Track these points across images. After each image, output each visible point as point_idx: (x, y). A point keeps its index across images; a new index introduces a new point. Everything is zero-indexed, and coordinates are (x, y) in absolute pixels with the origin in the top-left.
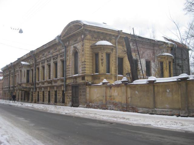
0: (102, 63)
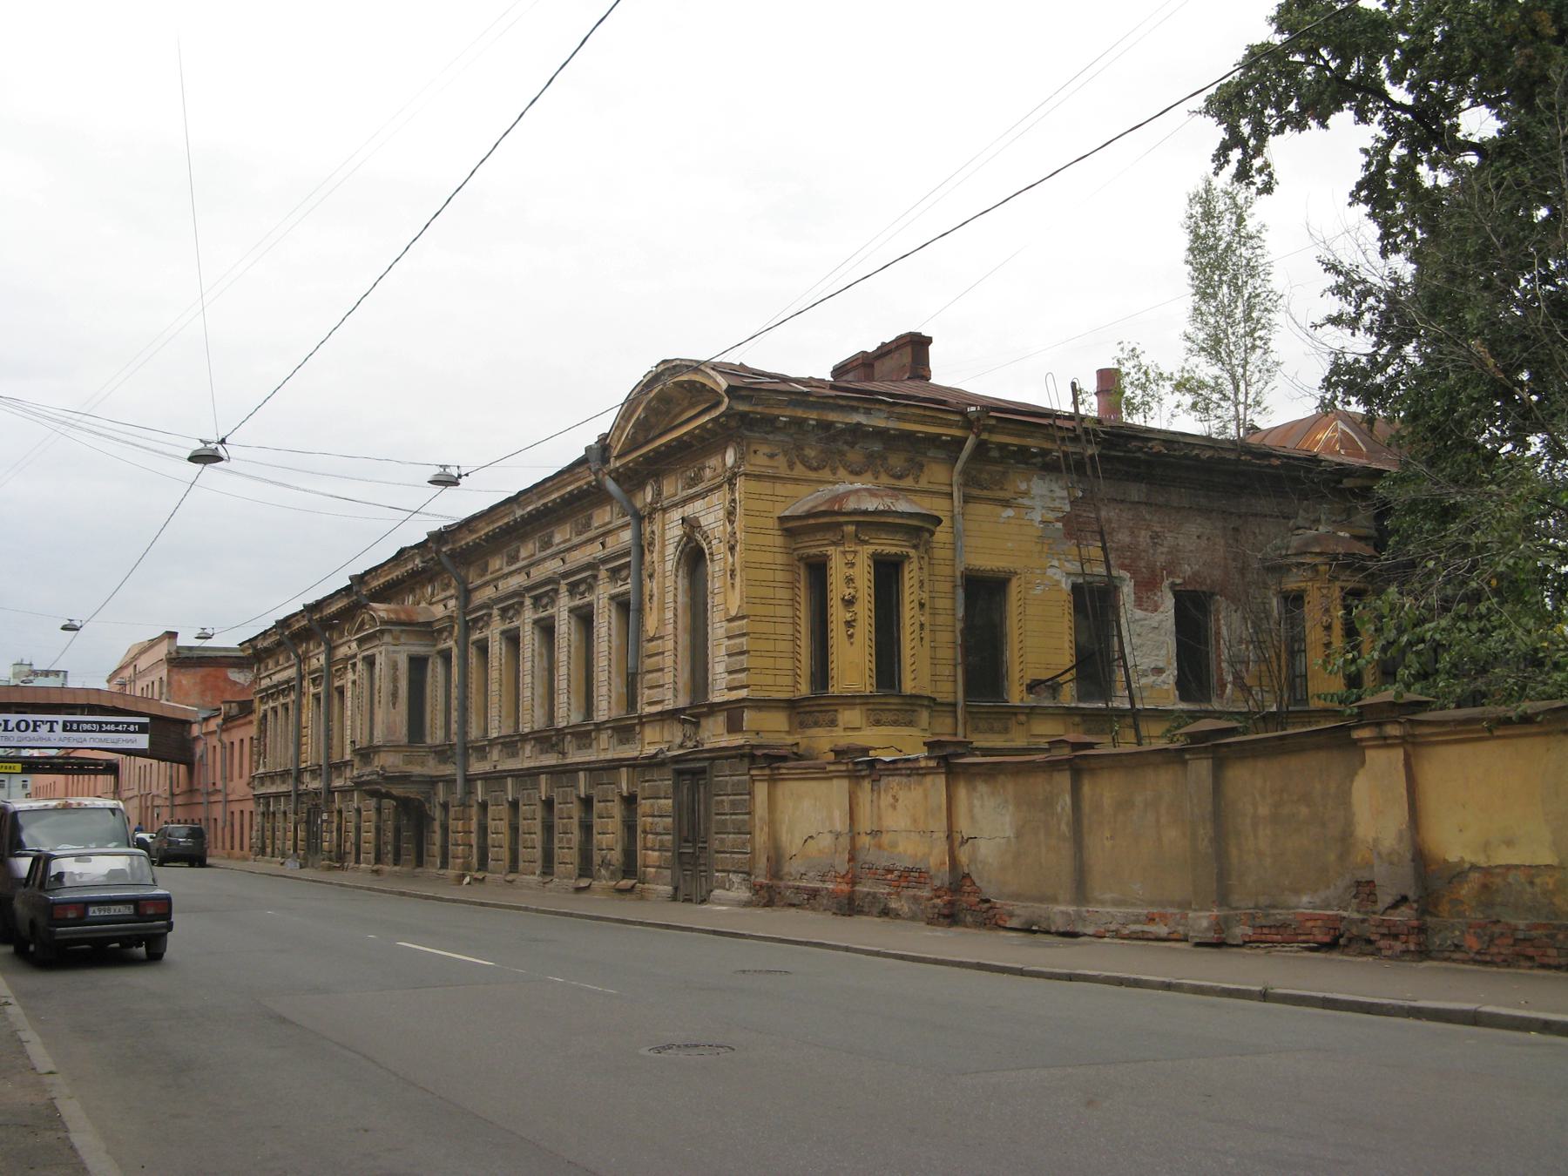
0: (849, 624)
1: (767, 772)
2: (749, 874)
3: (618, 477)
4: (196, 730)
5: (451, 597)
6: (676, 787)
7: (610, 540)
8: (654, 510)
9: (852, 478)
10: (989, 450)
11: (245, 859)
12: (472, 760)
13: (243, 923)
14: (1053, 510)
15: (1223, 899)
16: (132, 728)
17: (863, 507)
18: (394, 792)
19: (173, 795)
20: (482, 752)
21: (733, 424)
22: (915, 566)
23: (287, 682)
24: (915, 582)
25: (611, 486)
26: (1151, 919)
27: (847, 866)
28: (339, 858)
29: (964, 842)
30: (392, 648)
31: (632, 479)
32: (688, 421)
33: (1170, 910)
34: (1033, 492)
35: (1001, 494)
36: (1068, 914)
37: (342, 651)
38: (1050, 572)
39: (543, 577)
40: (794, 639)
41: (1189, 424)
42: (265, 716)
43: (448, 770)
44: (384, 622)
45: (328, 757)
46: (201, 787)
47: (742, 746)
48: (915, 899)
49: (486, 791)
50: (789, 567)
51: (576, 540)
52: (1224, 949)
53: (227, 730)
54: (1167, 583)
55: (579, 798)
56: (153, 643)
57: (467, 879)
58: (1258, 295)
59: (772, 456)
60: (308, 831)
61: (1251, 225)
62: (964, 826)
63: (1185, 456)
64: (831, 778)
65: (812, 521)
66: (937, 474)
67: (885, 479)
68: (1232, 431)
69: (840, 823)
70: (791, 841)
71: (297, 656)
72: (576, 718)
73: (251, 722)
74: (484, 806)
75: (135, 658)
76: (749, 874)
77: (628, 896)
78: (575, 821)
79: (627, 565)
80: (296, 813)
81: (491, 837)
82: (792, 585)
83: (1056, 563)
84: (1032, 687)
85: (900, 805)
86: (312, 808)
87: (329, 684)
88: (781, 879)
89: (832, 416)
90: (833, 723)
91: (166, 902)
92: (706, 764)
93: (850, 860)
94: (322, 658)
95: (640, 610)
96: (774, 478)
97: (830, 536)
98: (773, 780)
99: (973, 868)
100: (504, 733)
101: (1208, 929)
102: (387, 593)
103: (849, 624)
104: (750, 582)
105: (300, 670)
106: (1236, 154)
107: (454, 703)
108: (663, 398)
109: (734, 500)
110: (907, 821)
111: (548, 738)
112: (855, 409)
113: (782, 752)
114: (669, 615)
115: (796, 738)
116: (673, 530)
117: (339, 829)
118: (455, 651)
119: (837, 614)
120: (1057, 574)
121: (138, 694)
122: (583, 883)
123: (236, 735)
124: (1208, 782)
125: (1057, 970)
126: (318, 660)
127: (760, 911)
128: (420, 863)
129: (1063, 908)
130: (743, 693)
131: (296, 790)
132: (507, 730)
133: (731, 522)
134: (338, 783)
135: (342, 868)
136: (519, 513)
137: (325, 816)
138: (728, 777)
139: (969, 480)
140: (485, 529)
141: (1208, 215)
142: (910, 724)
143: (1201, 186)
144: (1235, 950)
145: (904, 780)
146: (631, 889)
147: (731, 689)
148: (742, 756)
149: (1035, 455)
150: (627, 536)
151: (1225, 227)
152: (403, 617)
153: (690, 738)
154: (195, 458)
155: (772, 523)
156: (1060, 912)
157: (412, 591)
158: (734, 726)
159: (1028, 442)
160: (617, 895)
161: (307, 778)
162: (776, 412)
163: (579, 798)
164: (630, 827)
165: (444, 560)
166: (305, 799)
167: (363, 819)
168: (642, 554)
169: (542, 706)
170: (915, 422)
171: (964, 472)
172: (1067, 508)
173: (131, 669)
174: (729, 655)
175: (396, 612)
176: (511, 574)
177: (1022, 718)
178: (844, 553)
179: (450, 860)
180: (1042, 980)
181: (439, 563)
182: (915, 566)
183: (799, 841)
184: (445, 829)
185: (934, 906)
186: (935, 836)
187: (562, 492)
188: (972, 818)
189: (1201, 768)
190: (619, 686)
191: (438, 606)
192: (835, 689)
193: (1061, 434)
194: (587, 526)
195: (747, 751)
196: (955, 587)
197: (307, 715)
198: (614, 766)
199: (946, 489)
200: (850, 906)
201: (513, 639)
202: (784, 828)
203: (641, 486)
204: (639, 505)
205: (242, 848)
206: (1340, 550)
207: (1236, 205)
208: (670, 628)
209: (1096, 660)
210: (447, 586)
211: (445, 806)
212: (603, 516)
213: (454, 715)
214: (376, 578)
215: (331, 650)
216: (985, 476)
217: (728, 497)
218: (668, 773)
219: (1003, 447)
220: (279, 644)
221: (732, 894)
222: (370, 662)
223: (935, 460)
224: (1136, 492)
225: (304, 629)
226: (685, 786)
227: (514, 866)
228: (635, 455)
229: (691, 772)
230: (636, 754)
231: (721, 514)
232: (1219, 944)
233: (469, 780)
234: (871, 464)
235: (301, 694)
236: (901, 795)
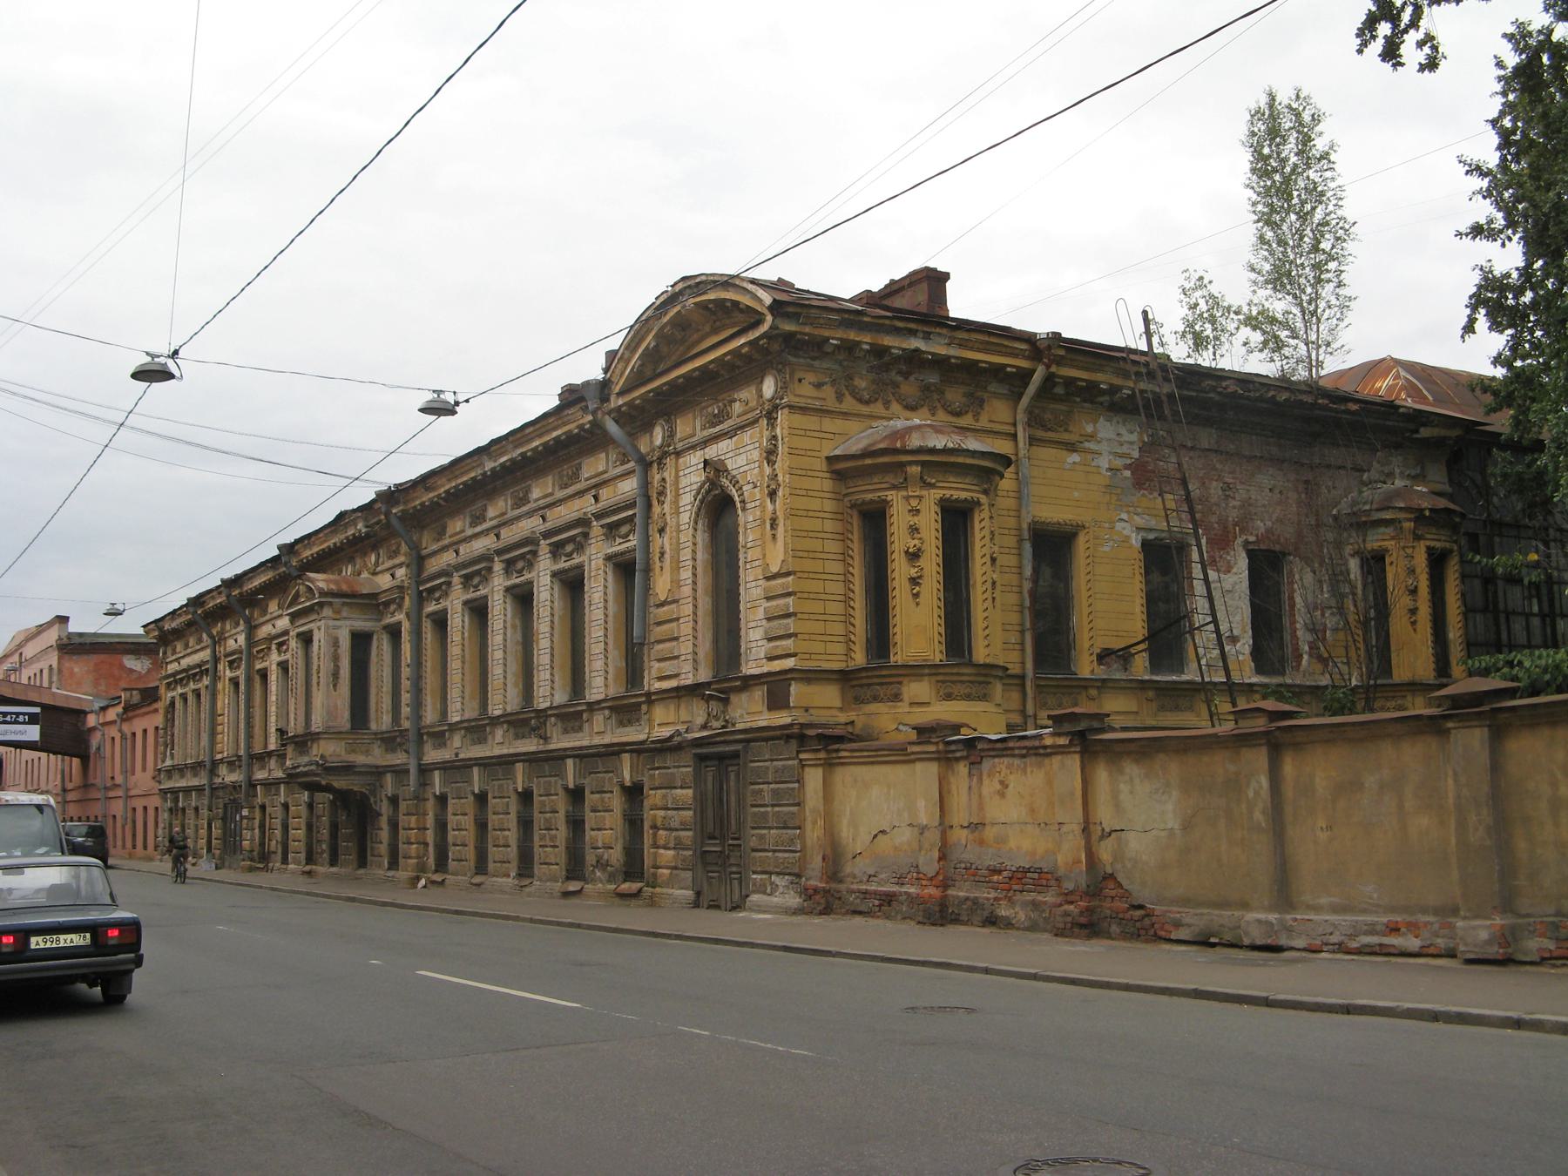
0: (914, 581)
1: (822, 755)
2: (799, 876)
3: (621, 417)
4: (92, 721)
5: (400, 565)
6: (698, 775)
7: (605, 493)
8: (665, 454)
9: (908, 414)
10: (1055, 384)
11: (150, 859)
12: (428, 747)
13: (232, 954)
14: (1121, 456)
15: (1507, 904)
16: (21, 718)
17: (930, 445)
18: (336, 784)
19: (64, 790)
20: (440, 738)
21: (776, 347)
22: (986, 514)
23: (199, 666)
24: (986, 532)
25: (612, 427)
26: (1394, 929)
27: (936, 866)
28: (262, 858)
29: (1106, 835)
30: (331, 623)
31: (638, 419)
32: (717, 344)
33: (1423, 918)
34: (1100, 435)
35: (1066, 437)
36: (1269, 923)
37: (265, 631)
38: (1119, 526)
39: (517, 538)
40: (847, 600)
41: (1261, 365)
42: (173, 704)
43: (398, 758)
44: (323, 593)
45: (249, 746)
46: (98, 781)
47: (790, 725)
48: (1035, 905)
49: (444, 782)
50: (839, 516)
51: (560, 494)
52: (1513, 968)
53: (128, 719)
54: (1239, 541)
55: (566, 789)
56: (41, 629)
57: (423, 882)
58: (1327, 224)
59: (818, 386)
60: (225, 828)
61: (1320, 145)
62: (1105, 815)
63: (1261, 399)
64: (913, 761)
65: (868, 461)
66: (998, 411)
67: (942, 415)
68: (1302, 374)
69: (925, 812)
70: (855, 836)
71: (211, 637)
72: (560, 698)
73: (156, 711)
74: (442, 800)
75: (20, 646)
76: (799, 876)
77: (634, 902)
78: (561, 815)
79: (630, 519)
80: (210, 810)
81: (451, 835)
82: (844, 537)
83: (1124, 516)
84: (1104, 656)
85: (1010, 791)
86: (230, 803)
87: (250, 666)
88: (841, 881)
89: (888, 341)
90: (897, 697)
91: (132, 929)
92: (739, 747)
93: (940, 859)
94: (242, 639)
95: (648, 570)
98: (829, 765)
99: (1118, 866)
100: (466, 716)
101: (1489, 942)
102: (324, 561)
103: (914, 581)
104: (797, 533)
105: (214, 651)
106: (1384, 29)
107: (406, 684)
108: (681, 323)
109: (775, 437)
110: (1024, 811)
111: (525, 721)
112: (913, 333)
113: (838, 732)
114: (686, 574)
115: (852, 716)
116: (690, 475)
117: (262, 826)
118: (406, 626)
119: (900, 570)
120: (1125, 529)
121: (25, 681)
122: (573, 886)
123: (138, 725)
124: (1484, 758)
125: (1320, 999)
126: (237, 640)
127: (817, 920)
128: (362, 862)
129: (1262, 916)
130: (789, 663)
131: (211, 784)
132: (472, 712)
133: (771, 463)
134: (260, 775)
135: (266, 869)
136: (489, 465)
137: (245, 812)
138: (765, 762)
139: (1034, 420)
140: (445, 486)
141: (1274, 133)
142: (984, 697)
143: (1263, 101)
144: (1528, 968)
145: (1017, 761)
146: (637, 894)
147: (770, 659)
148: (788, 737)
149: (1104, 392)
150: (629, 486)
151: (1290, 148)
152: (344, 587)
153: (717, 718)
154: (139, 375)
156: (1256, 920)
157: (351, 560)
158: (777, 701)
159: (1099, 377)
160: (617, 900)
161: (223, 769)
162: (826, 333)
163: (566, 789)
164: (634, 823)
165: (395, 522)
166: (221, 793)
167: (295, 812)
168: (649, 506)
169: (516, 685)
170: (979, 350)
171: (1029, 411)
172: (1136, 454)
173: (16, 658)
174: (769, 619)
175: (336, 582)
176: (476, 536)
177: (1093, 692)
178: (907, 498)
179: (401, 861)
180: (1305, 1014)
181: (388, 525)
182: (986, 514)
183: (864, 837)
184: (394, 826)
185: (1066, 914)
186: (1064, 829)
187: (546, 438)
188: (1117, 806)
189: (1471, 740)
190: (617, 660)
191: (384, 574)
192: (898, 657)
193: (1135, 369)
194: (575, 477)
195: (795, 730)
196: (1020, 541)
197: (224, 701)
198: (613, 752)
199: (1011, 429)
200: (941, 915)
201: (479, 611)
202: (845, 822)
203: (648, 427)
204: (643, 449)
205: (145, 848)
206: (1425, 505)
207: (1301, 124)
208: (687, 590)
209: (1167, 631)
210: (393, 554)
211: (394, 801)
212: (596, 465)
213: (406, 697)
214: (309, 546)
215: (251, 629)
216: (1048, 416)
217: (766, 434)
218: (687, 757)
219: (1070, 382)
220: (190, 624)
221: (776, 900)
222: (306, 639)
223: (996, 395)
224: (1207, 438)
225: (221, 607)
226: (710, 774)
227: (481, 867)
228: (643, 390)
229: (718, 758)
230: (642, 737)
231: (756, 455)
232: (1505, 962)
233: (425, 771)
234: (927, 399)
235: (216, 678)
236: (1013, 780)
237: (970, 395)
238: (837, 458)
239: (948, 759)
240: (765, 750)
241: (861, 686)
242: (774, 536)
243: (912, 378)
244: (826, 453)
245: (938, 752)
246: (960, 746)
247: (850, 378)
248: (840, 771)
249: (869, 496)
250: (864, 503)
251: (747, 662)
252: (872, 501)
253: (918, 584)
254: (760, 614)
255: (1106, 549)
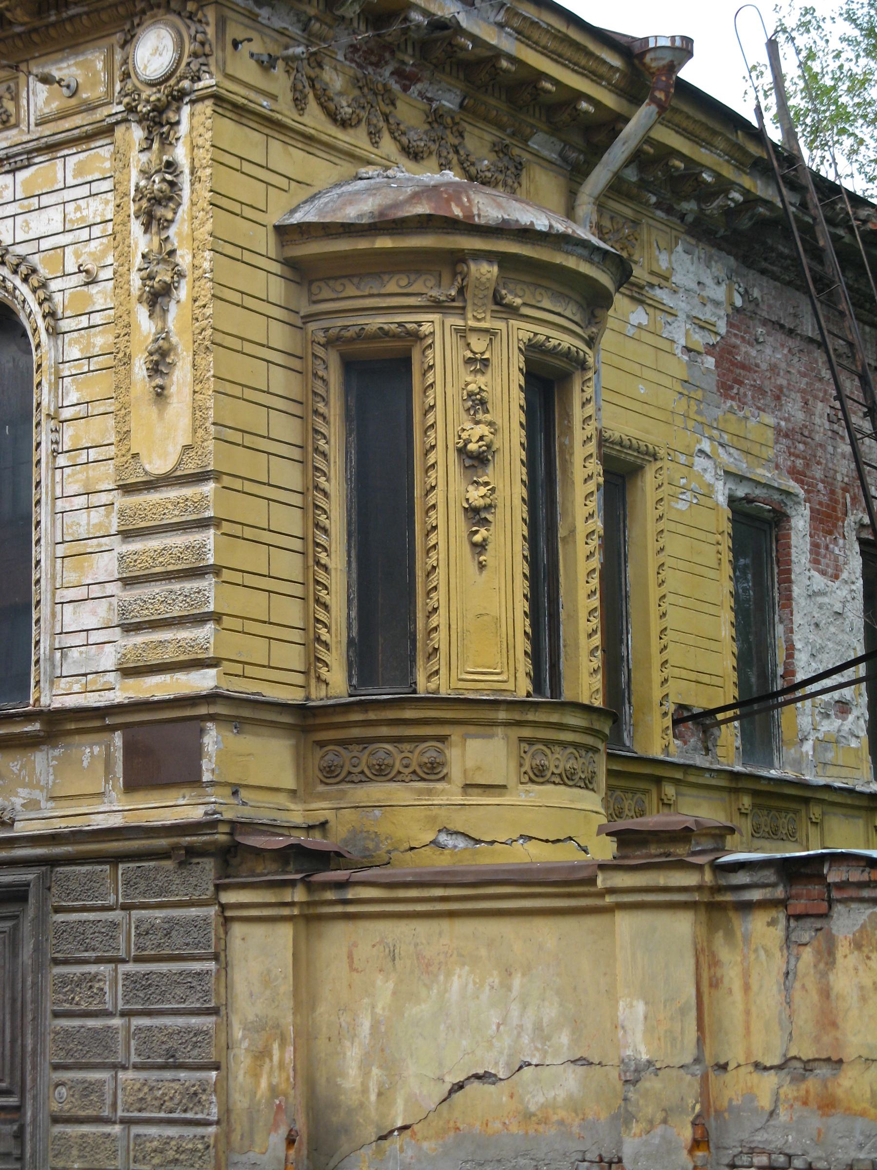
0: (476, 515)
1: (299, 895)
38: (700, 463)
47: (209, 825)
50: (301, 363)
65: (384, 243)
82: (307, 411)
83: (706, 446)
90: (433, 771)
92: (29, 876)
96: (272, 124)
97: (429, 288)
98: (310, 919)
103: (476, 515)
115: (321, 810)
119: (443, 490)
130: (203, 681)
133: (152, 221)
147: (128, 672)
155: (264, 242)
178: (462, 333)
202: (353, 1054)
217: (138, 160)
231: (100, 208)
237: (500, 150)
238: (305, 230)
239: (721, 907)
240: (113, 885)
241: (344, 743)
242: (160, 394)
243: (414, 90)
244: (276, 218)
245: (699, 888)
246: (769, 876)
247: (316, 61)
248: (339, 932)
249: (376, 322)
250: (362, 336)
251: (53, 680)
252: (382, 333)
253: (485, 522)
254: (105, 566)
255: (682, 506)
